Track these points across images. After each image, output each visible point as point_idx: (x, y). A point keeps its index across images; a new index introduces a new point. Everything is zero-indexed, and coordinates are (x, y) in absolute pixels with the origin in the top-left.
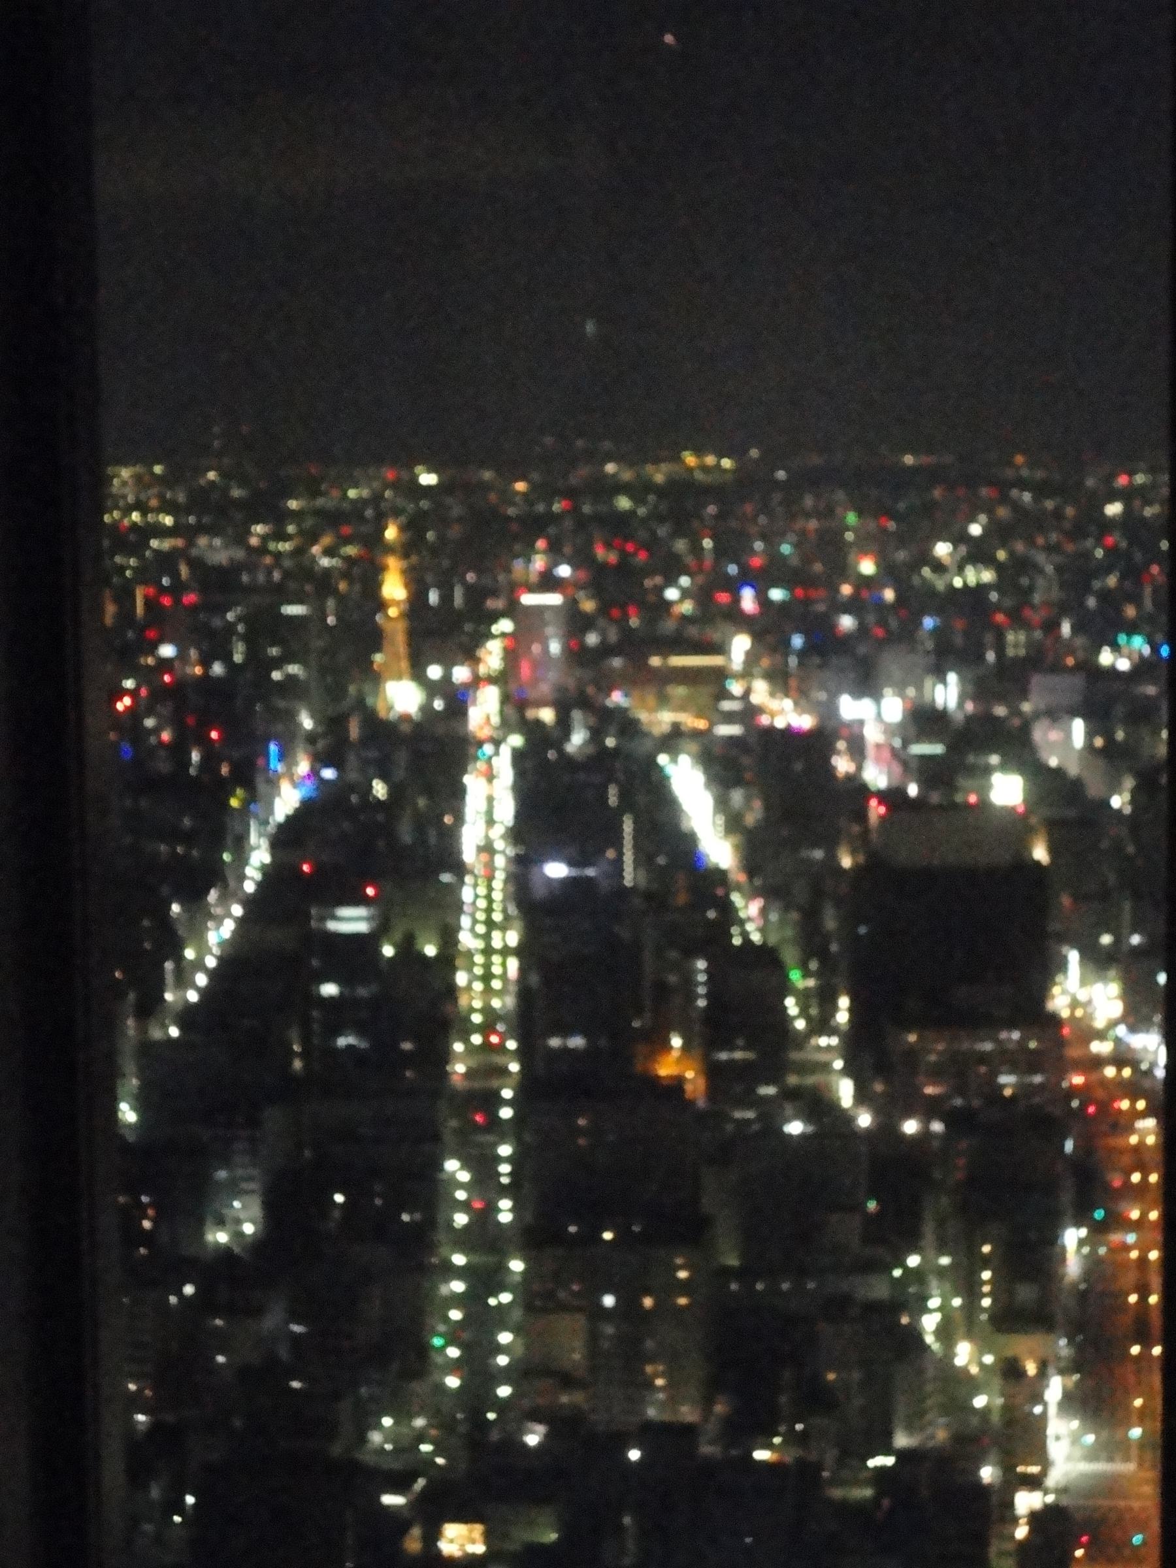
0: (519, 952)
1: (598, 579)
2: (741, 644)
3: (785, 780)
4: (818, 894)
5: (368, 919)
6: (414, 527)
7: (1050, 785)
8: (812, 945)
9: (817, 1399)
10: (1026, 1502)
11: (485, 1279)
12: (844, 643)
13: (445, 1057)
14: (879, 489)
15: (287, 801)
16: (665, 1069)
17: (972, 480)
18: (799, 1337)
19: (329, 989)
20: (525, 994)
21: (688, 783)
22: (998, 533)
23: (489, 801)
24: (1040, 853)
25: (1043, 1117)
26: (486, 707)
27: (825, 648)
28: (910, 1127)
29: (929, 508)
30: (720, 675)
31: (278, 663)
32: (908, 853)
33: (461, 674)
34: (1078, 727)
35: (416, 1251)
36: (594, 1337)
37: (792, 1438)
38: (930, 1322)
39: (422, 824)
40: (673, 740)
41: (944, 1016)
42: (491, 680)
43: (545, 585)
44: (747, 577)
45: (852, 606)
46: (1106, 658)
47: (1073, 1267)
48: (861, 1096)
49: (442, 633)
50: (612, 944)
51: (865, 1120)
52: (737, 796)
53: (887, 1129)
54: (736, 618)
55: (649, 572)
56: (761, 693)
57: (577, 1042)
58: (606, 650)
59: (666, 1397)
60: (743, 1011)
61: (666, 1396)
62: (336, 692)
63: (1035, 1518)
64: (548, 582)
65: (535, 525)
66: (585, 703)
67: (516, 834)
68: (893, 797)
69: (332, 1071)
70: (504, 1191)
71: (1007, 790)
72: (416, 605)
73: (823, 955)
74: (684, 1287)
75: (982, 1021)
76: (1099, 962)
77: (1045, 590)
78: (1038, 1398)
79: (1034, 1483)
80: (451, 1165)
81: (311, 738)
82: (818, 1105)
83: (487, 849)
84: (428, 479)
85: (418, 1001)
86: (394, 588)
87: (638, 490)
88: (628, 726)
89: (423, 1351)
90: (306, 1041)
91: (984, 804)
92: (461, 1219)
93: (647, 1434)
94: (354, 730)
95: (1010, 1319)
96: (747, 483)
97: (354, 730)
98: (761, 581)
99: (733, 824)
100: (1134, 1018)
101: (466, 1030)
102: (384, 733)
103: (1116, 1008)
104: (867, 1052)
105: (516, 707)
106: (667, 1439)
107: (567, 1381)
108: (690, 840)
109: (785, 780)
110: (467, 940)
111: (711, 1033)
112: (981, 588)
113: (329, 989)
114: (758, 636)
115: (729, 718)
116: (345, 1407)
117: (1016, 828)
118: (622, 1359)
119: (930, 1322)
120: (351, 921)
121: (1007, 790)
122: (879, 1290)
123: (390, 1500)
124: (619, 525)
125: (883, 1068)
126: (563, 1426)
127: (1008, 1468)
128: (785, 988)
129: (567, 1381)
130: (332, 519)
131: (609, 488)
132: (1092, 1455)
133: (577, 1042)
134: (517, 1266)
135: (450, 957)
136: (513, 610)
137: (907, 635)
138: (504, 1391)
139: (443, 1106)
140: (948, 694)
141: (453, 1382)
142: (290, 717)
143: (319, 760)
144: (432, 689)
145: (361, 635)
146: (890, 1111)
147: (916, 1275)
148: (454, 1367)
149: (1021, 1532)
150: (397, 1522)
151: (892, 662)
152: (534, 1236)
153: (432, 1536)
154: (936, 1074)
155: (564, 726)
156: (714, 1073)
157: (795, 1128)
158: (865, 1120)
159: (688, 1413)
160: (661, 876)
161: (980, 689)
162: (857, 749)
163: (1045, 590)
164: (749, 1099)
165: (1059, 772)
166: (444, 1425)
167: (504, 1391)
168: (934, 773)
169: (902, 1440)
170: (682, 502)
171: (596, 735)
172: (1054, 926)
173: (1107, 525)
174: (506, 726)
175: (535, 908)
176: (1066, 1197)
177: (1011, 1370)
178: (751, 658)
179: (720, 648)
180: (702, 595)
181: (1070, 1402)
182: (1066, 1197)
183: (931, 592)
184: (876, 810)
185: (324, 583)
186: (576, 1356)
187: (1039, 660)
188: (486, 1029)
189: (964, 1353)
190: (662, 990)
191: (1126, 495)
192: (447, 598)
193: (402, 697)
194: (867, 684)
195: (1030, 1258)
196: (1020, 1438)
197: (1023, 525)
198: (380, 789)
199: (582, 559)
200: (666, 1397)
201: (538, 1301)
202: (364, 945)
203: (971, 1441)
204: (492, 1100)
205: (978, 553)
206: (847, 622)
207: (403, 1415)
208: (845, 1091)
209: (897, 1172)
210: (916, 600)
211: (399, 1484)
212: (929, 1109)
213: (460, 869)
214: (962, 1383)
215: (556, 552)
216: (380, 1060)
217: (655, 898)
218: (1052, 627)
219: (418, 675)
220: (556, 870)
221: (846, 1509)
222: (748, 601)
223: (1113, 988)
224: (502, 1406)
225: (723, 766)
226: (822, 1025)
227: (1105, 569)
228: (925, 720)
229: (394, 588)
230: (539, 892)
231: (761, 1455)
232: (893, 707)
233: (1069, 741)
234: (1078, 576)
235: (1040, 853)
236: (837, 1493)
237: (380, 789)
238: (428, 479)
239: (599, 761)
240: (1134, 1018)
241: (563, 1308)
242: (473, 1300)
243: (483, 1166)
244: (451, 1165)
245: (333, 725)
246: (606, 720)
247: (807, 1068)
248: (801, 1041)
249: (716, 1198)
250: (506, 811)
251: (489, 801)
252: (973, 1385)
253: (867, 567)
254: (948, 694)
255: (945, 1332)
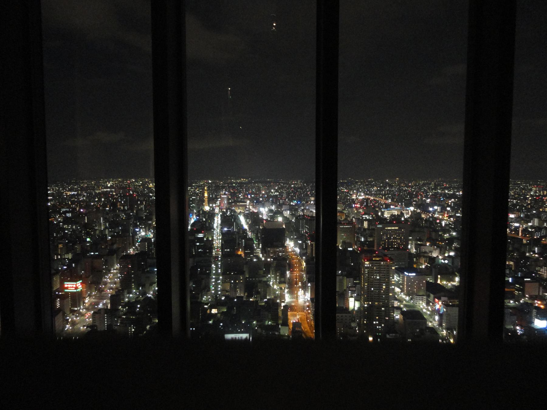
0: (221, 239)
1: (231, 194)
2: (248, 202)
3: (254, 218)
4: (258, 231)
5: (354, 309)
6: (208, 188)
7: (285, 218)
8: (257, 238)
9: (258, 293)
10: (283, 304)
11: (217, 279)
12: (261, 202)
13: (212, 252)
14: (265, 183)
15: (192, 221)
16: (239, 253)
17: (276, 182)
18: (255, 286)
19: (198, 244)
20: (222, 244)
21: (242, 219)
22: (279, 188)
23: (217, 220)
24: (284, 227)
25: (284, 259)
26: (217, 209)
27: (258, 202)
28: (269, 260)
29: (271, 186)
30: (246, 205)
31: (191, 204)
32: (269, 227)
33: (214, 205)
34: (288, 212)
35: (209, 276)
36: (231, 286)
37: (255, 297)
38: (271, 283)
39: (210, 223)
40: (240, 213)
41: (272, 246)
42: (218, 206)
43: (224, 195)
44: (249, 194)
45: (262, 197)
46: (292, 203)
47: (288, 276)
48: (263, 256)
49: (212, 200)
50: (232, 239)
51: (263, 259)
52: (248, 220)
53: (266, 260)
54: (248, 198)
55: (237, 193)
56: (251, 207)
57: (228, 250)
58: (232, 202)
59: (240, 293)
60: (249, 246)
61: (240, 293)
62: (199, 208)
63: (284, 306)
64: (225, 194)
65: (223, 187)
66: (229, 209)
67: (221, 225)
68: (266, 220)
69: (198, 254)
70: (220, 268)
71: (280, 219)
72: (209, 197)
73: (258, 239)
74: (241, 280)
75: (278, 247)
76: (291, 239)
77: (284, 195)
78: (284, 292)
79: (284, 302)
80: (213, 265)
81: (196, 213)
82: (258, 257)
83: (217, 227)
84: (210, 182)
85: (209, 245)
86: (206, 195)
87: (236, 183)
88: (235, 212)
89: (209, 288)
90: (195, 250)
91: (277, 221)
92: (214, 272)
93: (238, 298)
94: (201, 212)
95: (280, 283)
96: (250, 182)
97: (201, 212)
98: (251, 194)
99: (247, 223)
100: (295, 246)
101: (215, 249)
102: (205, 212)
103: (293, 245)
104: (264, 251)
105: (221, 209)
106: (239, 298)
107: (227, 291)
108: (242, 226)
109: (254, 218)
110: (215, 238)
111: (245, 248)
112: (277, 195)
113: (198, 244)
114: (250, 201)
115: (247, 211)
116: (200, 295)
117: (281, 224)
118: (234, 288)
119: (271, 283)
120: (201, 235)
121: (280, 219)
122: (265, 279)
123: (205, 306)
124: (234, 188)
125: (265, 253)
126: (227, 297)
127: (281, 301)
128: (254, 243)
129: (227, 291)
130: (199, 186)
131: (232, 183)
132: (290, 299)
133: (228, 250)
134: (221, 277)
135: (213, 240)
136: (220, 198)
137: (268, 201)
138: (219, 293)
139: (212, 258)
140: (273, 208)
141: (213, 292)
142: (193, 210)
143: (196, 216)
144: (210, 207)
145: (202, 201)
146: (266, 258)
147: (270, 278)
148: (213, 290)
149: (282, 308)
150: (207, 309)
151: (266, 204)
152: (223, 274)
153: (211, 311)
154: (272, 253)
155: (227, 211)
156: (245, 253)
157: (255, 260)
158: (263, 259)
159: (242, 295)
160: (239, 230)
161: (277, 207)
162: (262, 214)
163: (284, 195)
164: (250, 257)
165: (286, 217)
166: (212, 297)
167: (219, 293)
168: (272, 217)
169: (268, 297)
170: (241, 185)
171: (231, 213)
172: (286, 235)
173: (292, 188)
174: (219, 211)
175: (223, 234)
176: (287, 268)
177: (281, 289)
178: (249, 203)
179: (246, 202)
180: (244, 196)
181: (288, 292)
182: (287, 268)
183: (271, 195)
184: (264, 222)
185: (197, 194)
186: (228, 288)
187: (284, 204)
188: (217, 248)
189: (275, 287)
190: (239, 244)
191: (294, 184)
192: (212, 196)
193: (207, 208)
194: (264, 206)
195: (283, 275)
196: (282, 297)
197: (282, 188)
198: (204, 219)
199: (229, 191)
200: (240, 293)
201: (224, 282)
202: (203, 238)
203: (276, 297)
204: (218, 257)
205: (277, 191)
206: (261, 199)
207: (207, 296)
208: (261, 256)
209: (267, 265)
210: (269, 197)
211: (207, 304)
212: (271, 257)
213: (214, 229)
214: (275, 290)
215: (226, 190)
216: (205, 252)
217: (238, 233)
218: (285, 200)
219: (209, 206)
220: (226, 229)
221: (261, 306)
222: (249, 196)
223: (293, 243)
224: (219, 295)
225: (246, 216)
226: (258, 248)
227: (291, 193)
228: (271, 211)
229: (206, 195)
230: (224, 232)
231: (251, 300)
232: (267, 209)
233: (287, 213)
234: (288, 194)
235: (284, 227)
236: (260, 304)
237: (204, 219)
238: (210, 182)
239: (231, 216)
240: (295, 246)
241: (227, 282)
242: (216, 282)
243: (217, 265)
244: (213, 265)
245: (199, 212)
246: (232, 211)
247: (256, 253)
248: (255, 250)
249: (245, 269)
250: (220, 222)
251: (217, 220)
252: (276, 291)
253: (263, 192)
254: (273, 208)
255: (273, 284)
